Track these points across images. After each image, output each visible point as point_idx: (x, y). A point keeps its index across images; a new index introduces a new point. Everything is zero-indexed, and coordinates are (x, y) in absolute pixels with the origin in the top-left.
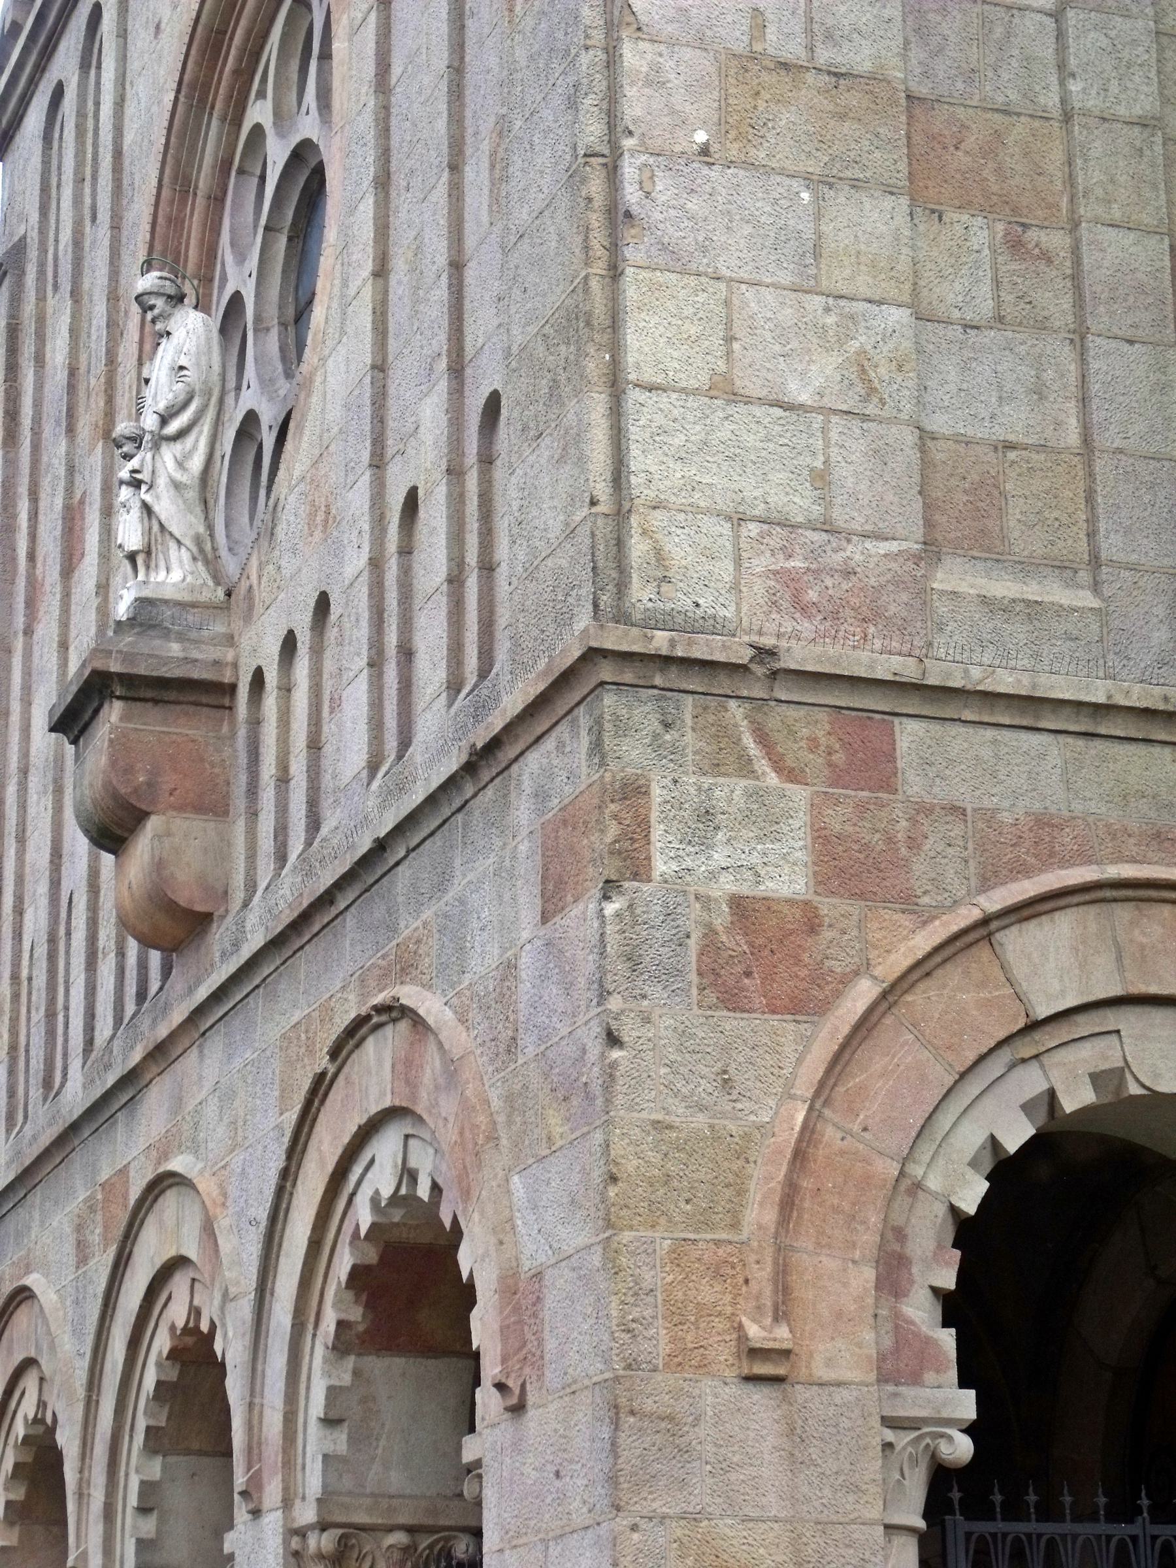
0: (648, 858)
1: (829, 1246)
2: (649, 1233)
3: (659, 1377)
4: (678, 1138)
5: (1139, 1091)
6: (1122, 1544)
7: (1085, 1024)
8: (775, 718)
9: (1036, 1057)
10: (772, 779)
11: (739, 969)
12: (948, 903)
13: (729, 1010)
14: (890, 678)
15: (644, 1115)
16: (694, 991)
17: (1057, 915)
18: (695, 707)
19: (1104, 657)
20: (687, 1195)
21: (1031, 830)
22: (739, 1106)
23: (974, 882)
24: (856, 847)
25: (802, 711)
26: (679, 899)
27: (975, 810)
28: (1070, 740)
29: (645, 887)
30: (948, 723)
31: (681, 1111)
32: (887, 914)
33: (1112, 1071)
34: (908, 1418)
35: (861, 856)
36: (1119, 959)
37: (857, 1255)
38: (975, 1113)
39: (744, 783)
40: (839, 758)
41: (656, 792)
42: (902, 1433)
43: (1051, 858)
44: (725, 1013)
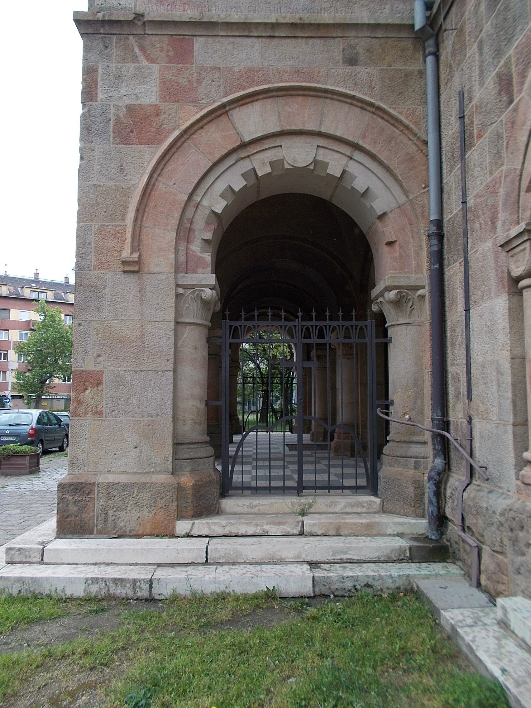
0: (97, 94)
1: (158, 225)
2: (90, 223)
3: (92, 272)
4: (102, 190)
5: (289, 167)
6: (321, 328)
7: (267, 144)
8: (147, 42)
9: (248, 156)
10: (145, 63)
11: (129, 130)
12: (211, 102)
13: (124, 144)
14: (188, 20)
15: (90, 182)
16: (111, 139)
17: (254, 103)
18: (117, 39)
19: (280, 9)
20: (105, 210)
21: (246, 73)
22: (126, 178)
23: (222, 93)
24: (176, 84)
25: (157, 38)
26: (107, 107)
27: (223, 68)
28: (264, 40)
29: (95, 104)
30: (214, 37)
31: (103, 181)
32: (187, 107)
33: (279, 160)
34: (188, 285)
35: (178, 87)
36: (279, 117)
37: (169, 228)
38: (222, 178)
39: (133, 65)
40: (171, 53)
41: (100, 70)
42: (186, 290)
43: (253, 82)
44: (123, 146)
